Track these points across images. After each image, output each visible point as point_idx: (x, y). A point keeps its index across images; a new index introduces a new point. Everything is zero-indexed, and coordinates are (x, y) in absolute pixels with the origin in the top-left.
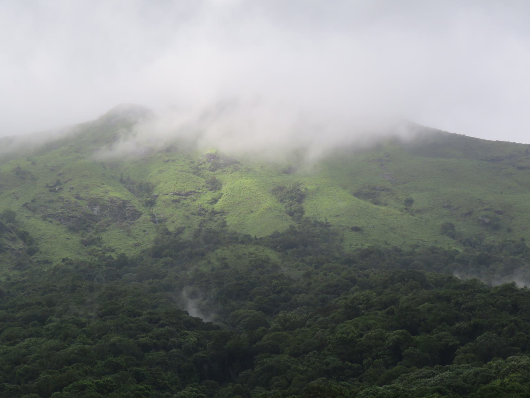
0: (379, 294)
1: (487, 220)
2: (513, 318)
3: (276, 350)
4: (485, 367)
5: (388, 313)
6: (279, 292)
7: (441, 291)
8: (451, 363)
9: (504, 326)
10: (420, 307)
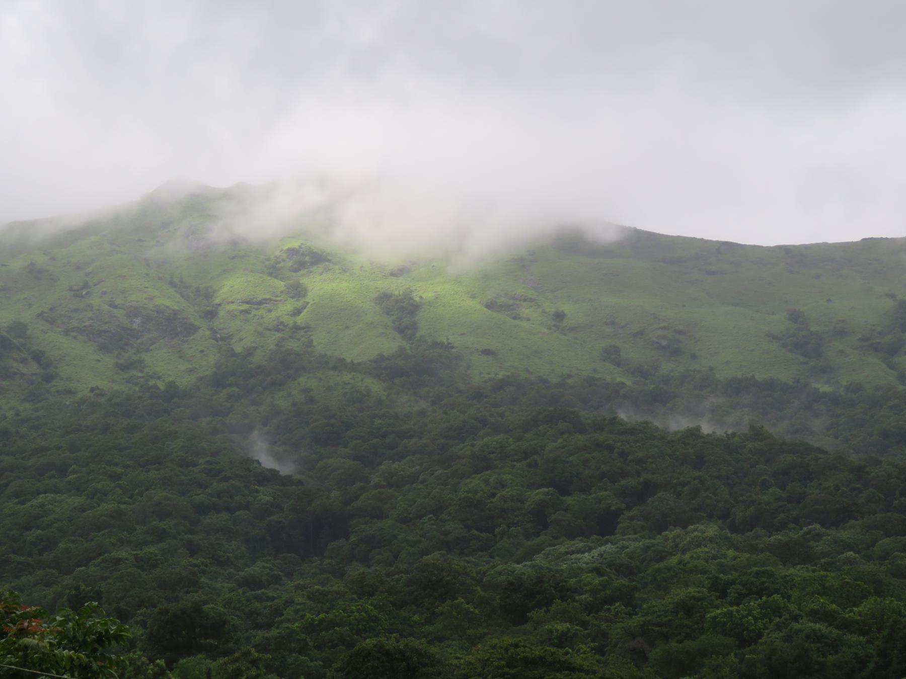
1: (664, 343)
2: (697, 473)
3: (380, 515)
4: (659, 539)
6: (384, 436)
10: (572, 458)
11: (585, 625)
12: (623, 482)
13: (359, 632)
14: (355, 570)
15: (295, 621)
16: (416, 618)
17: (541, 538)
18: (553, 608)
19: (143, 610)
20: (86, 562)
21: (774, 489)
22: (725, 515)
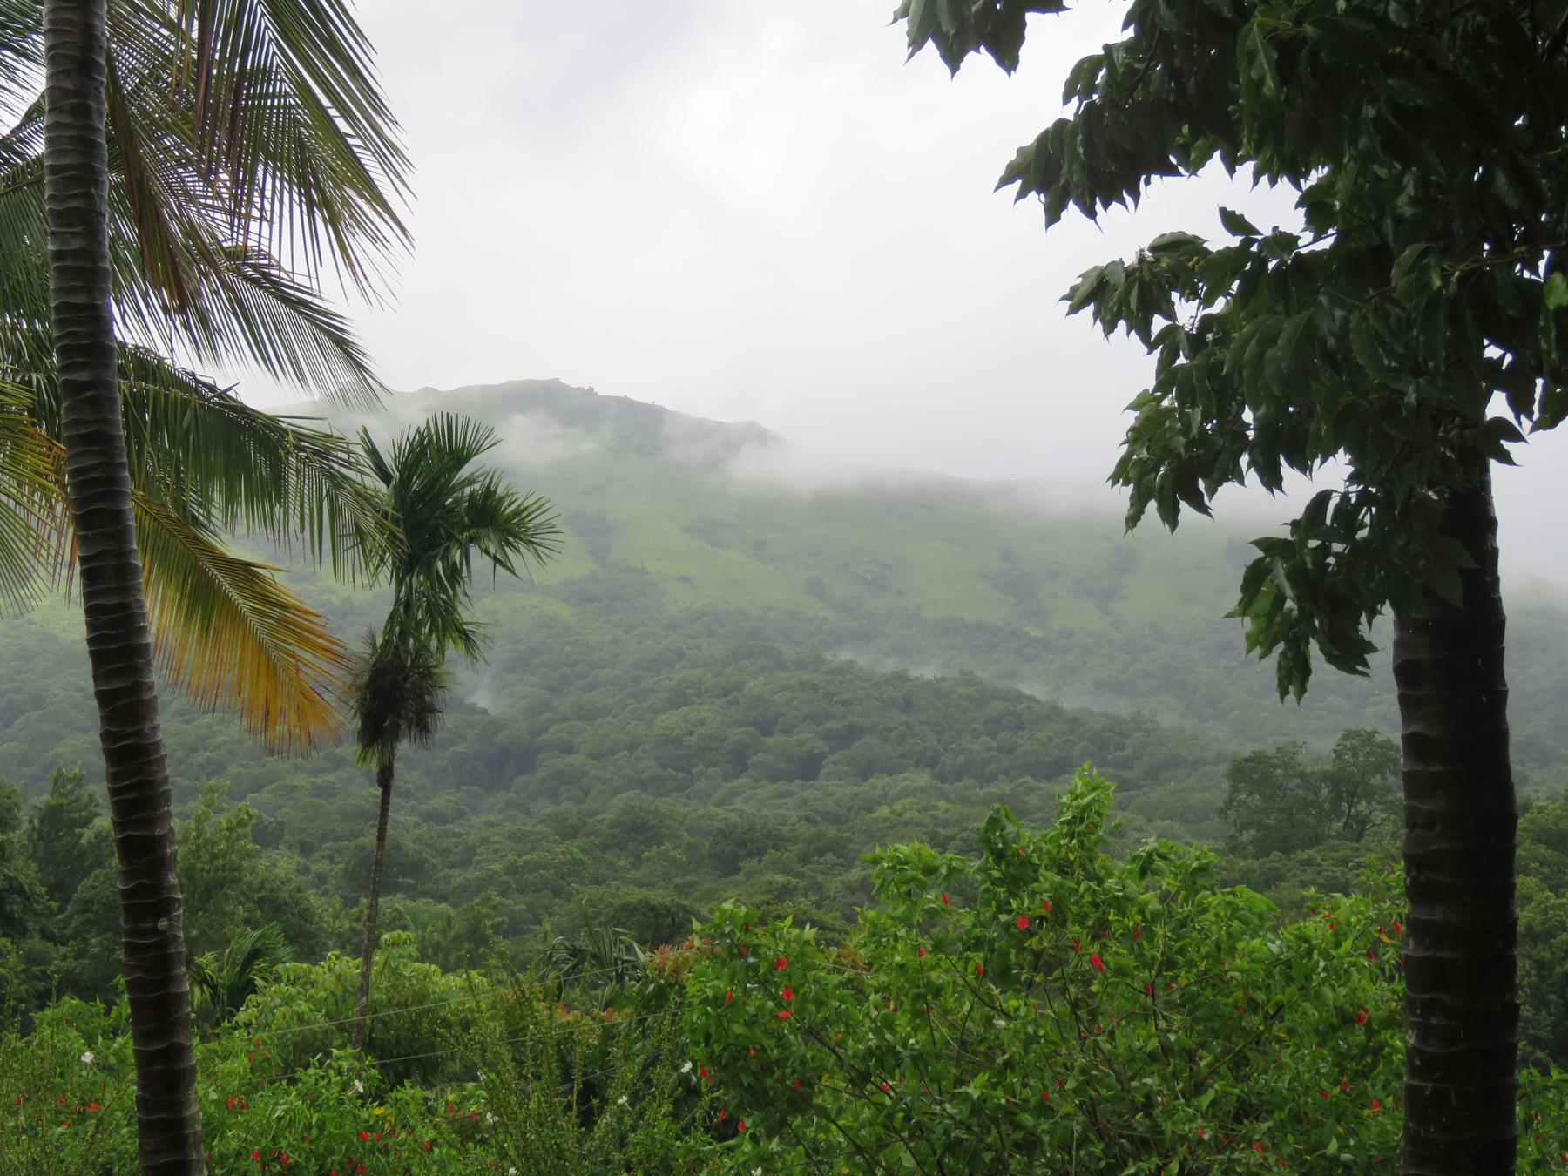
0: (718, 674)
1: (870, 577)
2: (904, 718)
3: (569, 749)
4: (864, 787)
5: (730, 703)
6: (573, 665)
7: (806, 676)
8: (815, 778)
9: (891, 730)
10: (775, 697)
11: (800, 875)
12: (828, 725)
13: (563, 877)
14: (544, 807)
15: (494, 861)
16: (622, 863)
17: (741, 781)
18: (767, 857)
19: (329, 844)
20: (258, 788)
21: (984, 738)
22: (932, 763)
